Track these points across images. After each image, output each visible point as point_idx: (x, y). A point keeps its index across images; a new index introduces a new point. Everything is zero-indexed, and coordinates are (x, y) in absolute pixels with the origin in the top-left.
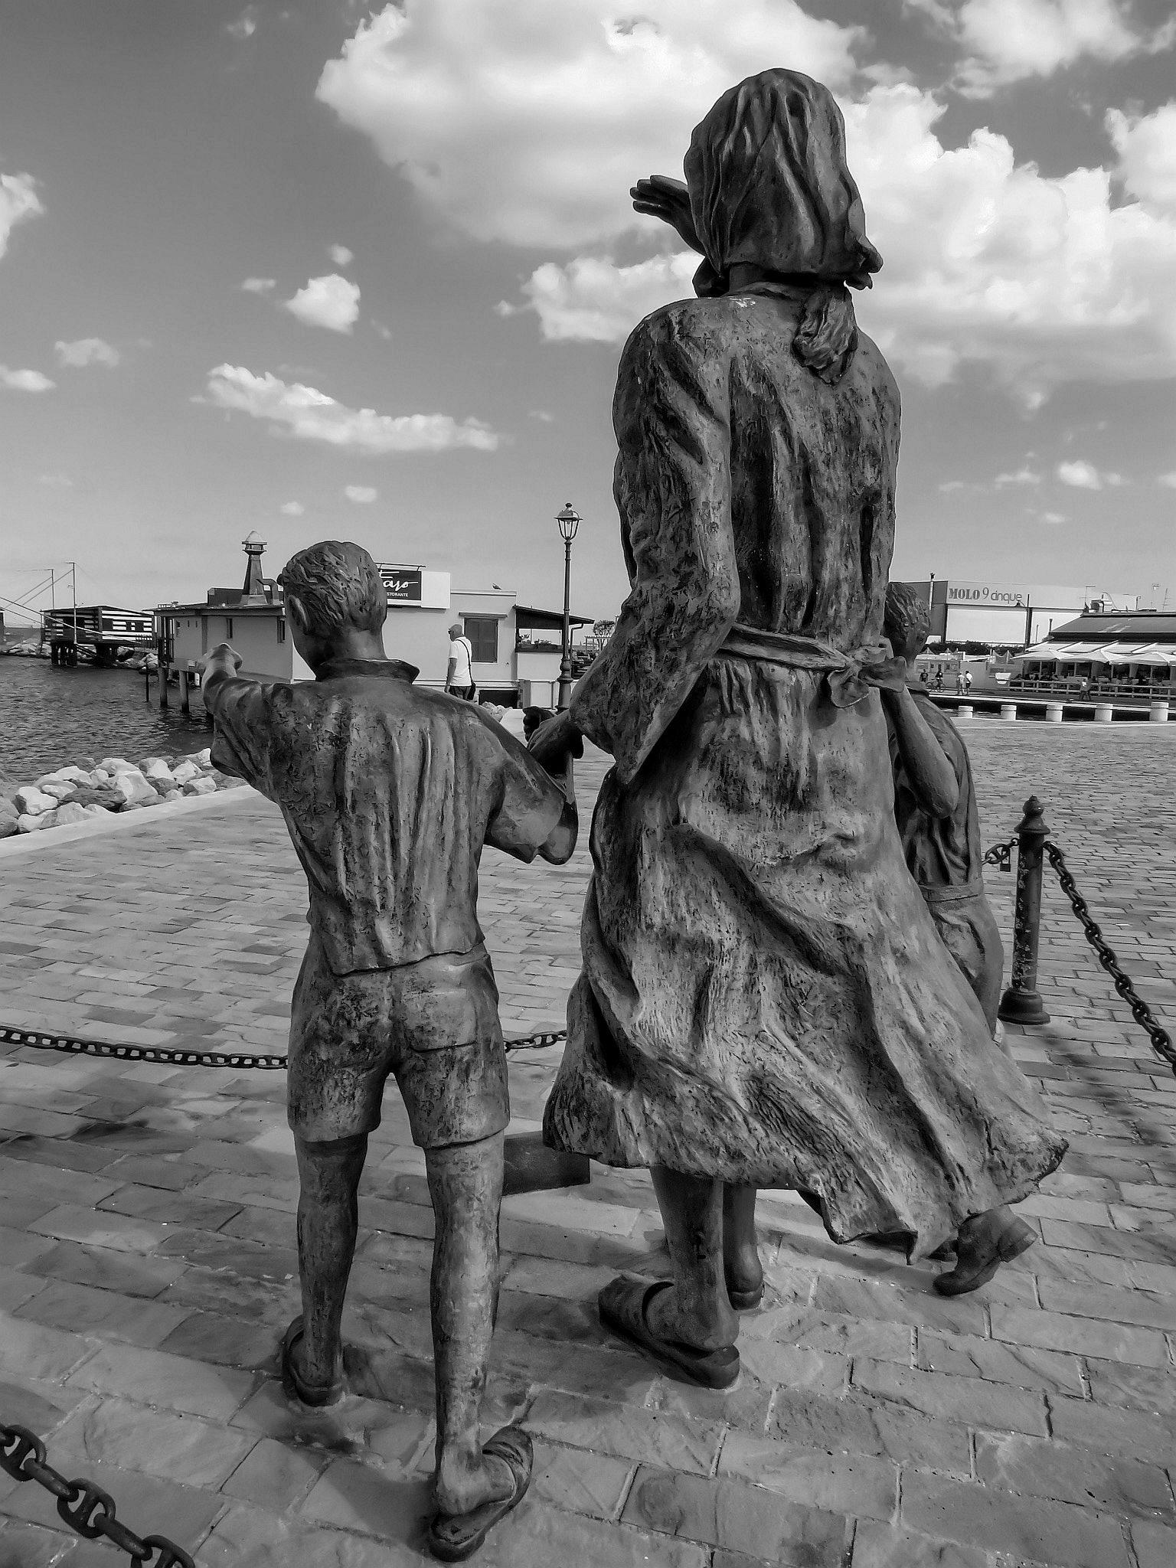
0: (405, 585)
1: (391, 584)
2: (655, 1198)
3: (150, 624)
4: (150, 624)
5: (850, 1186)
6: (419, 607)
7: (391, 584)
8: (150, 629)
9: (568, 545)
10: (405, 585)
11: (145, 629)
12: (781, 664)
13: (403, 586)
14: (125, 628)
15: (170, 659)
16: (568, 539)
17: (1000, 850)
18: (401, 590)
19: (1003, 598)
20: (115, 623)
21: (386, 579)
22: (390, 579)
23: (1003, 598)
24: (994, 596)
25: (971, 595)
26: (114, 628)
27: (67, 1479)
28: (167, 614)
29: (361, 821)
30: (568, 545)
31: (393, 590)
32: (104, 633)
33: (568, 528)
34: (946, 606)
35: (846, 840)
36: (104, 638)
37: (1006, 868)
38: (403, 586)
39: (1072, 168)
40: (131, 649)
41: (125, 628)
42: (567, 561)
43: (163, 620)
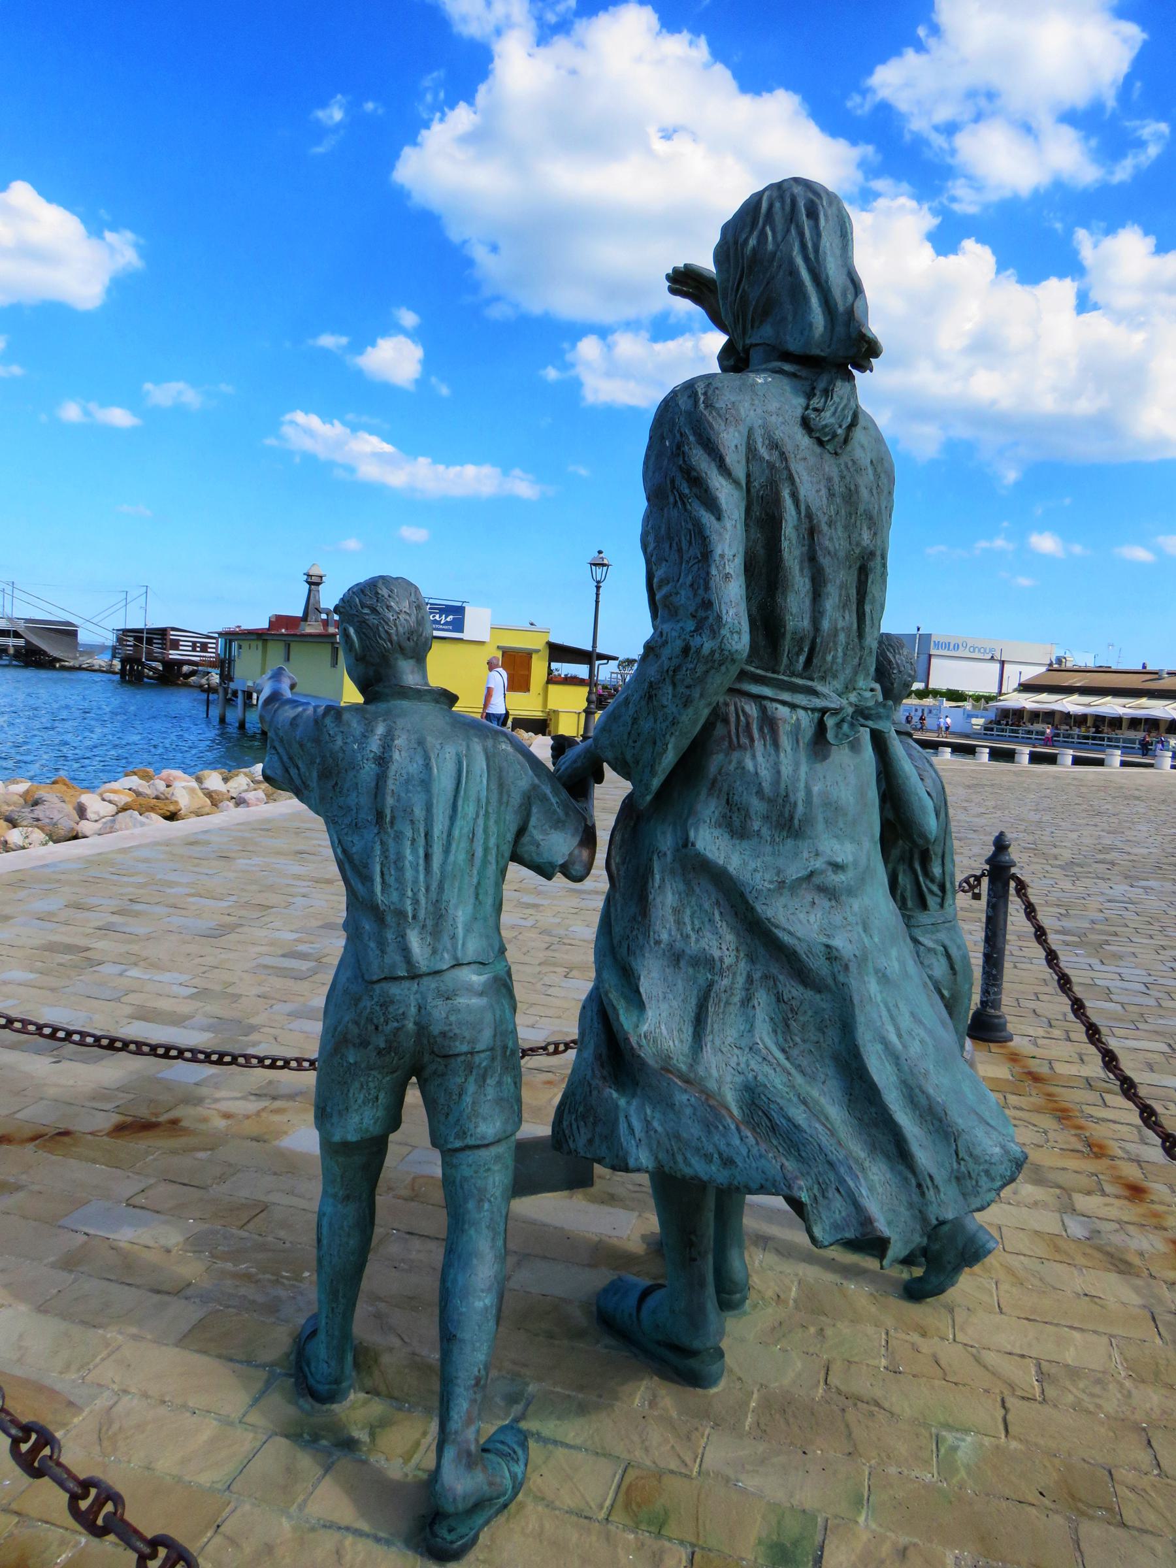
0: (450, 618)
3: (214, 646)
4: (214, 646)
5: (831, 1193)
9: (598, 588)
10: (450, 618)
11: (209, 650)
13: (448, 619)
14: (190, 648)
15: (231, 679)
16: (598, 582)
17: (972, 880)
18: (446, 623)
19: (979, 651)
20: (181, 643)
23: (979, 651)
24: (972, 649)
25: (952, 647)
26: (181, 648)
28: (230, 636)
29: (399, 836)
30: (598, 588)
31: (438, 622)
32: (171, 652)
33: (599, 571)
34: (930, 656)
36: (171, 657)
37: (977, 897)
38: (448, 619)
41: (190, 648)
42: (597, 602)
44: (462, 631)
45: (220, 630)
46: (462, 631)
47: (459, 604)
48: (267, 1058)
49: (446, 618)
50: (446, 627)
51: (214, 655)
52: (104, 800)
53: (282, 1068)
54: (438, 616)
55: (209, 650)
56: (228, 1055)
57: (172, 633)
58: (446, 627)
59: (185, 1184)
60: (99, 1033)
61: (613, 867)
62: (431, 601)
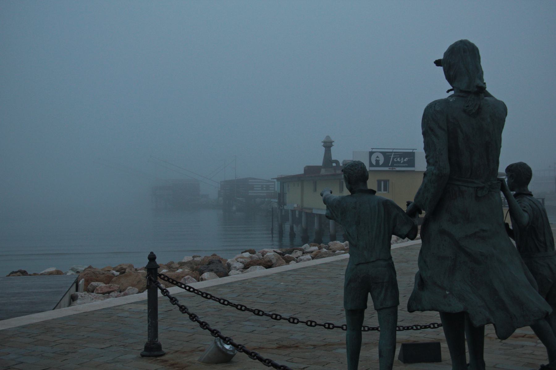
0: (406, 159)
1: (399, 160)
2: (446, 341)
3: (273, 186)
4: (273, 186)
6: (414, 171)
7: (399, 160)
8: (273, 189)
10: (406, 159)
11: (270, 189)
12: (465, 186)
13: (405, 160)
15: (285, 204)
18: (404, 163)
21: (395, 157)
22: (398, 157)
27: (302, 173)
28: (284, 181)
31: (399, 162)
32: (250, 191)
35: (484, 231)
36: (250, 194)
38: (405, 160)
39: (483, 79)
40: (263, 200)
41: (260, 189)
43: (281, 184)
44: (414, 167)
45: (276, 177)
46: (414, 167)
47: (411, 151)
48: (406, 327)
49: (404, 159)
50: (404, 165)
51: (273, 192)
52: (238, 262)
53: (410, 329)
54: (399, 159)
55: (270, 189)
56: (410, 327)
57: (250, 181)
58: (404, 165)
59: (304, 358)
60: (421, 325)
61: (142, 291)
62: (395, 151)
